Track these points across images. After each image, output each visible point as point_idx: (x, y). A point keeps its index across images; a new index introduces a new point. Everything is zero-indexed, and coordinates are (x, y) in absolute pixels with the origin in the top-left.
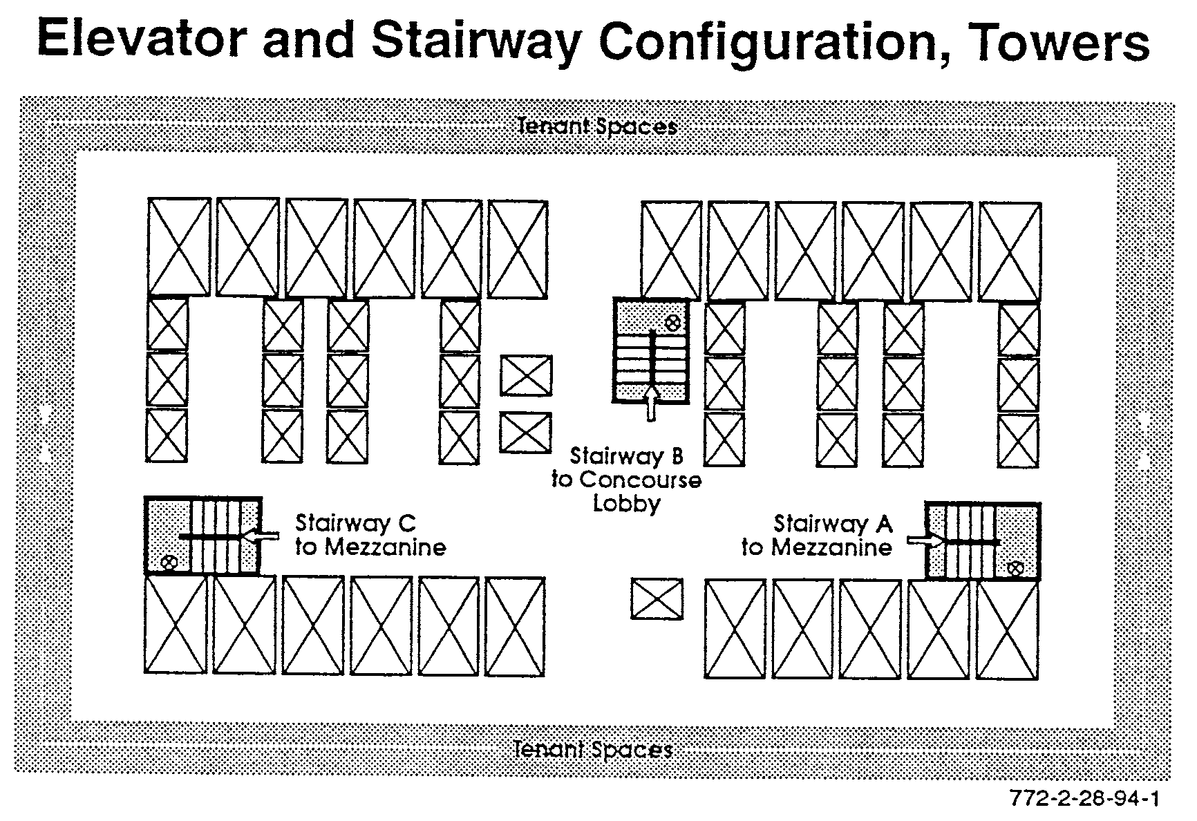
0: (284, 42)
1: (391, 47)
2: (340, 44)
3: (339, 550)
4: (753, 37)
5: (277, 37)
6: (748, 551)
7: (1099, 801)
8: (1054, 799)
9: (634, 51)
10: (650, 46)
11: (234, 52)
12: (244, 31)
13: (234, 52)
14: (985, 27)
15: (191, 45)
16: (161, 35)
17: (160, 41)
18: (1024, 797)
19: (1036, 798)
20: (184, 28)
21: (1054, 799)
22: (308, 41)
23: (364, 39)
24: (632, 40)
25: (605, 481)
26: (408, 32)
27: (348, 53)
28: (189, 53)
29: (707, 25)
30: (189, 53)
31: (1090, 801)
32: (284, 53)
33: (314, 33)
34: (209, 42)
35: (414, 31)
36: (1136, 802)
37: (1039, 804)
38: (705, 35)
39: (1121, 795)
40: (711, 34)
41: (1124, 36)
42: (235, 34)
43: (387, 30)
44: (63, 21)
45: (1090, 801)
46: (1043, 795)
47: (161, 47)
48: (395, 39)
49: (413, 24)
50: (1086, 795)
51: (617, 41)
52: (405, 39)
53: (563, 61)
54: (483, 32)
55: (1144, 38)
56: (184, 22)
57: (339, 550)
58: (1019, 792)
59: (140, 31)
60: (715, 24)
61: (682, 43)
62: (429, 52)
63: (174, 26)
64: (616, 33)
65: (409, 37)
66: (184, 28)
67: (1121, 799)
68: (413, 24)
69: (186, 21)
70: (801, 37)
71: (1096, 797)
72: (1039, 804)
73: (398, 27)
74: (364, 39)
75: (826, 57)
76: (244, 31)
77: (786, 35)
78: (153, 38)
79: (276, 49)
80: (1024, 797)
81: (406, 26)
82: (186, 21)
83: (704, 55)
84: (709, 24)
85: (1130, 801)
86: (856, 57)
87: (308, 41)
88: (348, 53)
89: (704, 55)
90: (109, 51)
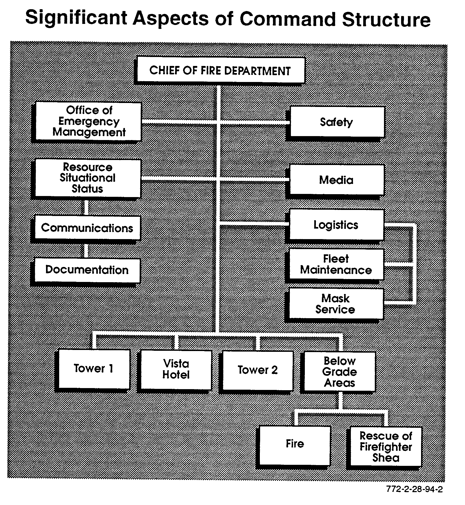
0: (309, 20)
1: (349, 23)
2: (330, 21)
3: (328, 300)
4: (53, 15)
5: (306, 18)
6: (101, 272)
9: (253, 22)
10: (259, 20)
16: (103, 17)
17: (103, 19)
18: (392, 488)
19: (396, 489)
21: (403, 489)
22: (318, 20)
23: (339, 19)
24: (252, 18)
25: (54, 229)
26: (356, 17)
27: (333, 24)
28: (398, 26)
29: (79, 11)
30: (398, 26)
31: (416, 490)
32: (309, 24)
33: (321, 17)
35: (358, 16)
36: (433, 491)
37: (397, 491)
38: (77, 14)
39: (428, 488)
40: (80, 15)
41: (421, 18)
43: (348, 16)
46: (399, 488)
47: (103, 21)
48: (351, 19)
49: (358, 14)
50: (415, 488)
52: (355, 20)
54: (368, 17)
55: (206, 16)
57: (328, 300)
58: (390, 486)
60: (81, 11)
61: (115, 18)
62: (303, 24)
63: (120, 14)
65: (122, 17)
67: (428, 489)
68: (358, 14)
69: (125, 12)
70: (415, 18)
71: (419, 489)
72: (397, 491)
73: (352, 15)
74: (339, 19)
75: (102, 23)
77: (409, 18)
78: (303, 20)
80: (392, 488)
81: (355, 15)
82: (125, 12)
83: (77, 22)
84: (79, 11)
85: (431, 490)
86: (360, 25)
87: (318, 20)
88: (333, 24)
89: (77, 22)
90: (428, 25)
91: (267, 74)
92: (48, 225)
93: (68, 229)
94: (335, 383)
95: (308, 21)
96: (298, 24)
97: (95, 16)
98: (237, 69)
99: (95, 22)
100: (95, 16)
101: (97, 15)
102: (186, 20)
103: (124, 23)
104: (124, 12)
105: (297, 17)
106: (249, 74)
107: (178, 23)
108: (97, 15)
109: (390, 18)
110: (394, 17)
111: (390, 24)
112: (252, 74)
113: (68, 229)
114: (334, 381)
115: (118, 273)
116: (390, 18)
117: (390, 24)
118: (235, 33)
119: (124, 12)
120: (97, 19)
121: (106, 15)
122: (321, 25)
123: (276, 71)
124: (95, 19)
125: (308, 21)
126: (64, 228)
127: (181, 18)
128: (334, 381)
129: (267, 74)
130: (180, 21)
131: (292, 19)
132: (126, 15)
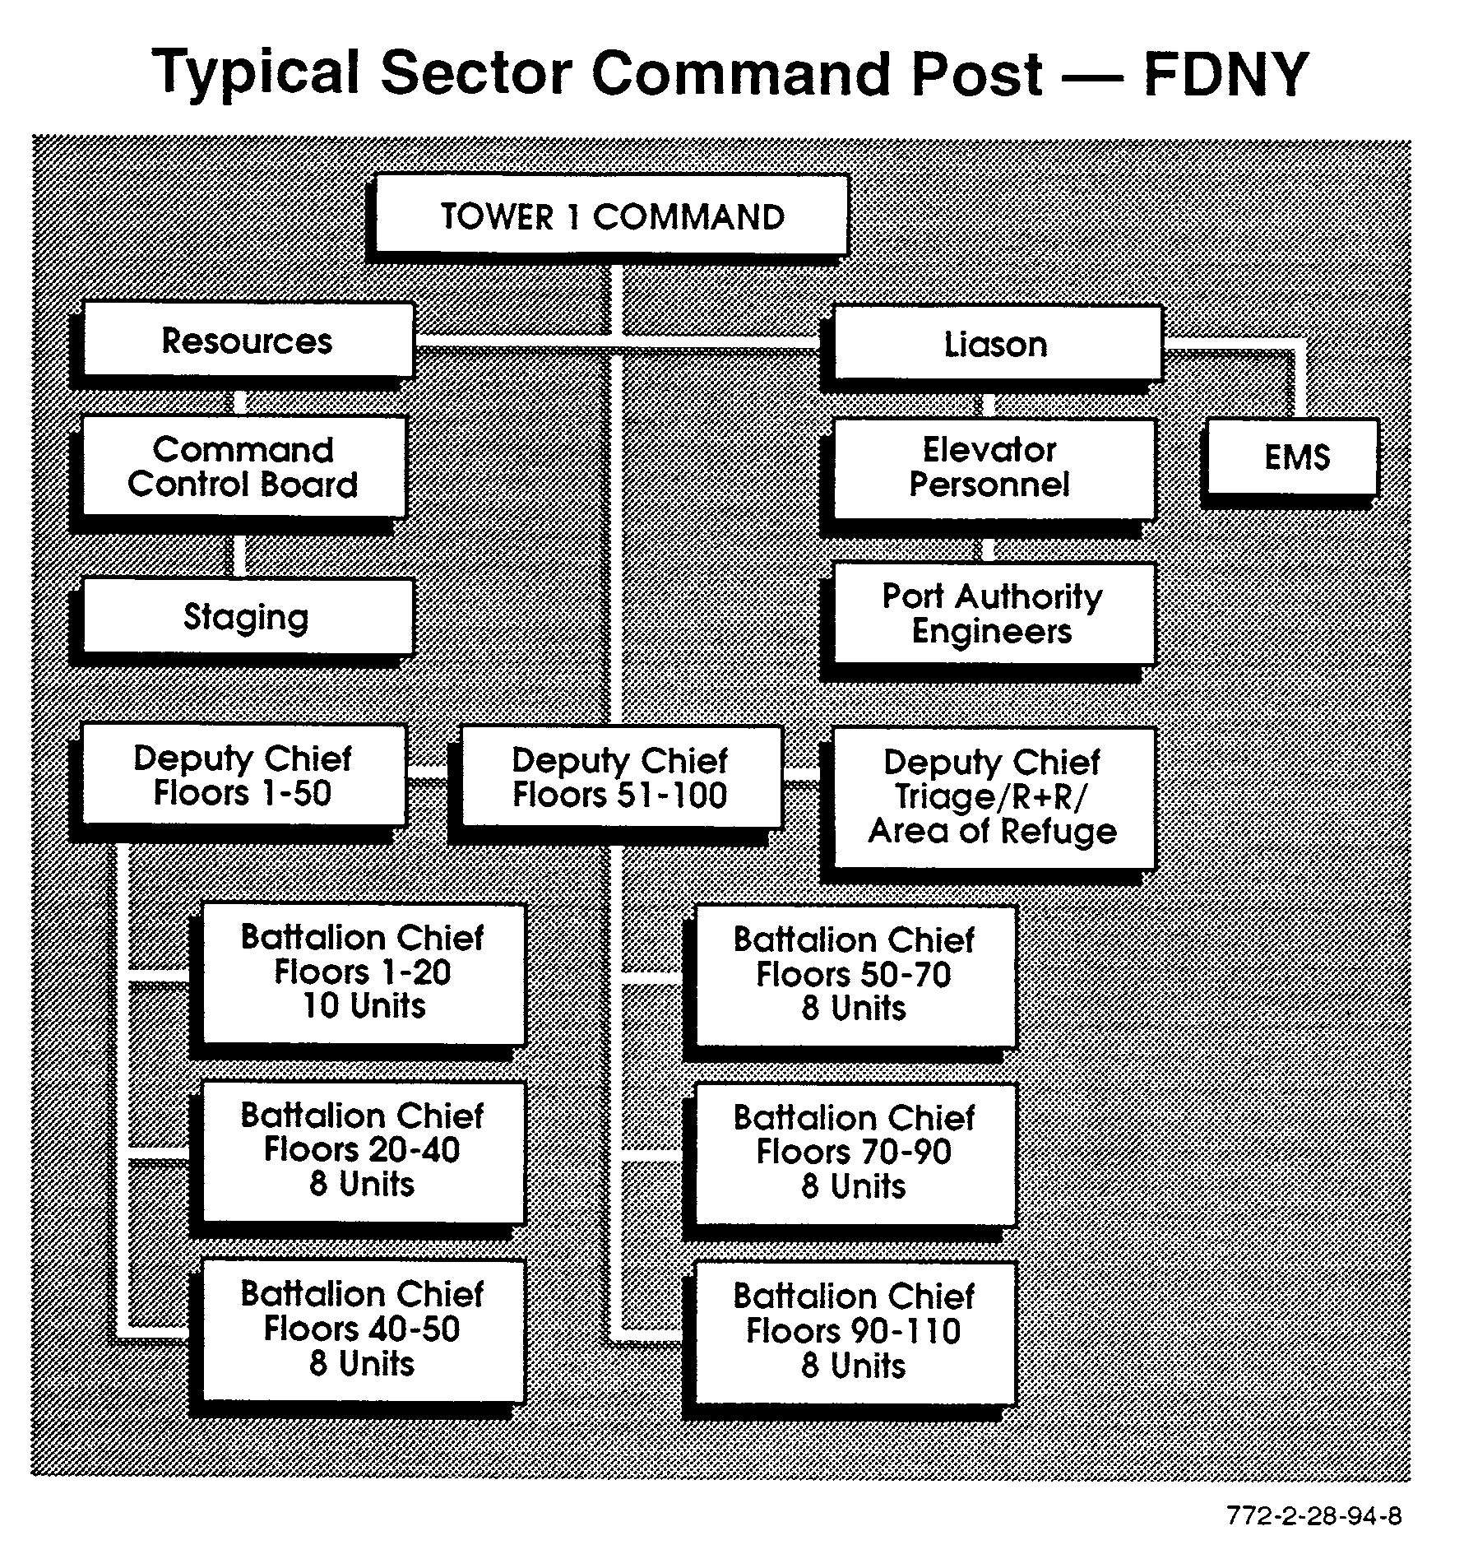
0: (808, 77)
7: (1330, 1519)
8: (1278, 1517)
9: (634, 85)
10: (653, 78)
11: (557, 89)
12: (569, 64)
13: (557, 89)
14: (170, 54)
15: (508, 80)
16: (799, 72)
17: (326, 75)
19: (1257, 1516)
20: (499, 62)
21: (1278, 1517)
22: (836, 76)
23: (371, 71)
24: (631, 72)
27: (883, 89)
28: (506, 90)
30: (506, 90)
31: (1320, 1519)
32: (808, 89)
34: (529, 77)
36: (1373, 1520)
37: (1260, 1522)
39: (1355, 1513)
42: (558, 67)
43: (399, 61)
44: (1173, 56)
45: (1320, 1519)
48: (405, 73)
51: (614, 72)
53: (195, 94)
56: (499, 54)
59: (212, 63)
63: (1021, 61)
64: (612, 63)
66: (499, 62)
72: (1260, 1522)
74: (371, 71)
75: (322, 90)
76: (569, 64)
79: (798, 85)
85: (1366, 1519)
87: (836, 76)
88: (883, 89)
91: (695, 225)
92: (175, 441)
93: (236, 455)
94: (902, 831)
95: (803, 79)
96: (774, 90)
97: (302, 66)
98: (533, 212)
99: (302, 84)
100: (302, 66)
101: (310, 65)
102: (472, 77)
103: (1035, 90)
104: (1033, 57)
105: (716, 67)
106: (732, 227)
107: (447, 88)
108: (310, 65)
109: (481, 68)
110: (1027, 66)
111: (481, 86)
112: (539, 227)
113: (236, 455)
114: (898, 827)
115: (1042, 592)
116: (481, 68)
117: (481, 86)
118: (576, 112)
119: (1033, 57)
120: (308, 76)
121: (808, 68)
122: (846, 91)
123: (529, 217)
124: (303, 76)
125: (803, 79)
126: (225, 451)
127: (455, 73)
128: (898, 827)
129: (695, 225)
130: (454, 82)
131: (753, 73)
132: (1040, 66)
